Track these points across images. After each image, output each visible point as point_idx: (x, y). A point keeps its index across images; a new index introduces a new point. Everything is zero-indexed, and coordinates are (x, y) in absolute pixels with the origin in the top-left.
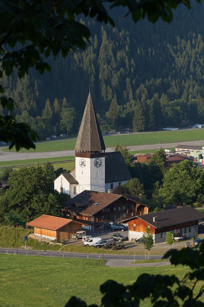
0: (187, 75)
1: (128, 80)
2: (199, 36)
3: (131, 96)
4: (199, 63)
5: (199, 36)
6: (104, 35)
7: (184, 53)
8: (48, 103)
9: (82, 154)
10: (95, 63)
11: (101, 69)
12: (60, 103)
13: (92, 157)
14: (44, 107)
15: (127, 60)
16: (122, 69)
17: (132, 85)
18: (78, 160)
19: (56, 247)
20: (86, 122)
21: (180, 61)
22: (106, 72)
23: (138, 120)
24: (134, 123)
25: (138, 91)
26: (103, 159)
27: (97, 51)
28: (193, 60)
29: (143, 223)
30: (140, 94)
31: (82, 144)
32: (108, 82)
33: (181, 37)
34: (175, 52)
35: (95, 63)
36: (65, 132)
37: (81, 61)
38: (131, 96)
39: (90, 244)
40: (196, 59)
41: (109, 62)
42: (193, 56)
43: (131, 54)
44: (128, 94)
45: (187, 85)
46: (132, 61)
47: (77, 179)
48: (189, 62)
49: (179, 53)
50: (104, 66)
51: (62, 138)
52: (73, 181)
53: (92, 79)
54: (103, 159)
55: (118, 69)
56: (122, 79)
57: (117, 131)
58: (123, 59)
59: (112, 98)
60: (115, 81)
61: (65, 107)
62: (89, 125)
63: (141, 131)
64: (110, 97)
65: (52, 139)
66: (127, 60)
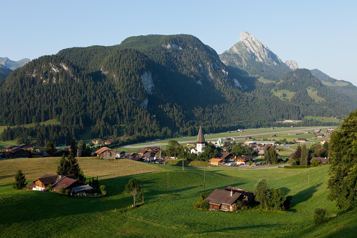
0: (199, 120)
1: (183, 121)
2: (201, 107)
3: (185, 126)
4: (202, 115)
5: (201, 107)
6: (175, 107)
7: (197, 113)
8: (163, 128)
9: (199, 143)
10: (173, 116)
11: (175, 118)
12: (166, 128)
13: (202, 144)
14: (162, 129)
15: (182, 115)
16: (181, 118)
17: (185, 123)
18: (198, 144)
19: (219, 166)
20: (200, 134)
21: (196, 115)
22: (177, 119)
23: (189, 133)
24: (188, 134)
25: (186, 124)
26: (204, 144)
27: (173, 112)
28: (200, 115)
29: (241, 160)
30: (187, 125)
31: (199, 140)
32: (178, 121)
33: (196, 108)
34: (195, 112)
35: (173, 116)
36: (169, 137)
37: (169, 115)
38: (185, 126)
39: (228, 165)
40: (201, 114)
41: (177, 116)
42: (200, 113)
43: (183, 113)
44: (184, 125)
45: (200, 122)
46: (184, 115)
47: (197, 150)
48: (199, 115)
49: (196, 113)
50: (176, 117)
51: (169, 139)
52: (196, 151)
53: (173, 121)
54: (204, 144)
55: (180, 118)
56: (182, 120)
57: (184, 136)
58: (181, 115)
59: (78, 125)
60: (180, 121)
61: (168, 129)
62: (201, 135)
63: (190, 136)
64: (179, 126)
65: (166, 139)
66: (182, 115)
